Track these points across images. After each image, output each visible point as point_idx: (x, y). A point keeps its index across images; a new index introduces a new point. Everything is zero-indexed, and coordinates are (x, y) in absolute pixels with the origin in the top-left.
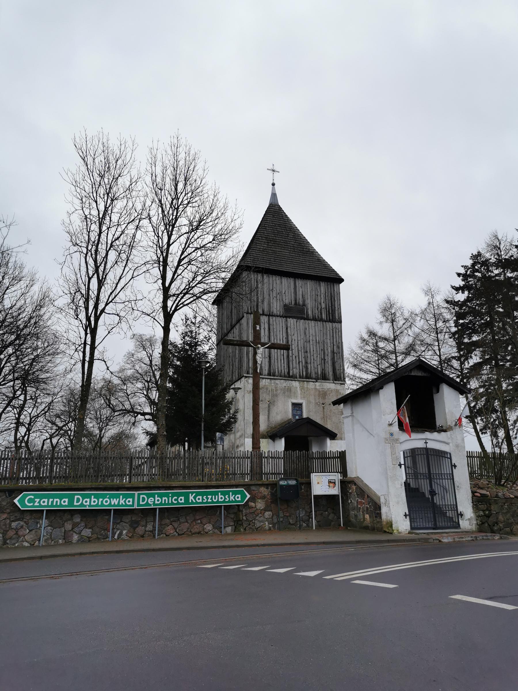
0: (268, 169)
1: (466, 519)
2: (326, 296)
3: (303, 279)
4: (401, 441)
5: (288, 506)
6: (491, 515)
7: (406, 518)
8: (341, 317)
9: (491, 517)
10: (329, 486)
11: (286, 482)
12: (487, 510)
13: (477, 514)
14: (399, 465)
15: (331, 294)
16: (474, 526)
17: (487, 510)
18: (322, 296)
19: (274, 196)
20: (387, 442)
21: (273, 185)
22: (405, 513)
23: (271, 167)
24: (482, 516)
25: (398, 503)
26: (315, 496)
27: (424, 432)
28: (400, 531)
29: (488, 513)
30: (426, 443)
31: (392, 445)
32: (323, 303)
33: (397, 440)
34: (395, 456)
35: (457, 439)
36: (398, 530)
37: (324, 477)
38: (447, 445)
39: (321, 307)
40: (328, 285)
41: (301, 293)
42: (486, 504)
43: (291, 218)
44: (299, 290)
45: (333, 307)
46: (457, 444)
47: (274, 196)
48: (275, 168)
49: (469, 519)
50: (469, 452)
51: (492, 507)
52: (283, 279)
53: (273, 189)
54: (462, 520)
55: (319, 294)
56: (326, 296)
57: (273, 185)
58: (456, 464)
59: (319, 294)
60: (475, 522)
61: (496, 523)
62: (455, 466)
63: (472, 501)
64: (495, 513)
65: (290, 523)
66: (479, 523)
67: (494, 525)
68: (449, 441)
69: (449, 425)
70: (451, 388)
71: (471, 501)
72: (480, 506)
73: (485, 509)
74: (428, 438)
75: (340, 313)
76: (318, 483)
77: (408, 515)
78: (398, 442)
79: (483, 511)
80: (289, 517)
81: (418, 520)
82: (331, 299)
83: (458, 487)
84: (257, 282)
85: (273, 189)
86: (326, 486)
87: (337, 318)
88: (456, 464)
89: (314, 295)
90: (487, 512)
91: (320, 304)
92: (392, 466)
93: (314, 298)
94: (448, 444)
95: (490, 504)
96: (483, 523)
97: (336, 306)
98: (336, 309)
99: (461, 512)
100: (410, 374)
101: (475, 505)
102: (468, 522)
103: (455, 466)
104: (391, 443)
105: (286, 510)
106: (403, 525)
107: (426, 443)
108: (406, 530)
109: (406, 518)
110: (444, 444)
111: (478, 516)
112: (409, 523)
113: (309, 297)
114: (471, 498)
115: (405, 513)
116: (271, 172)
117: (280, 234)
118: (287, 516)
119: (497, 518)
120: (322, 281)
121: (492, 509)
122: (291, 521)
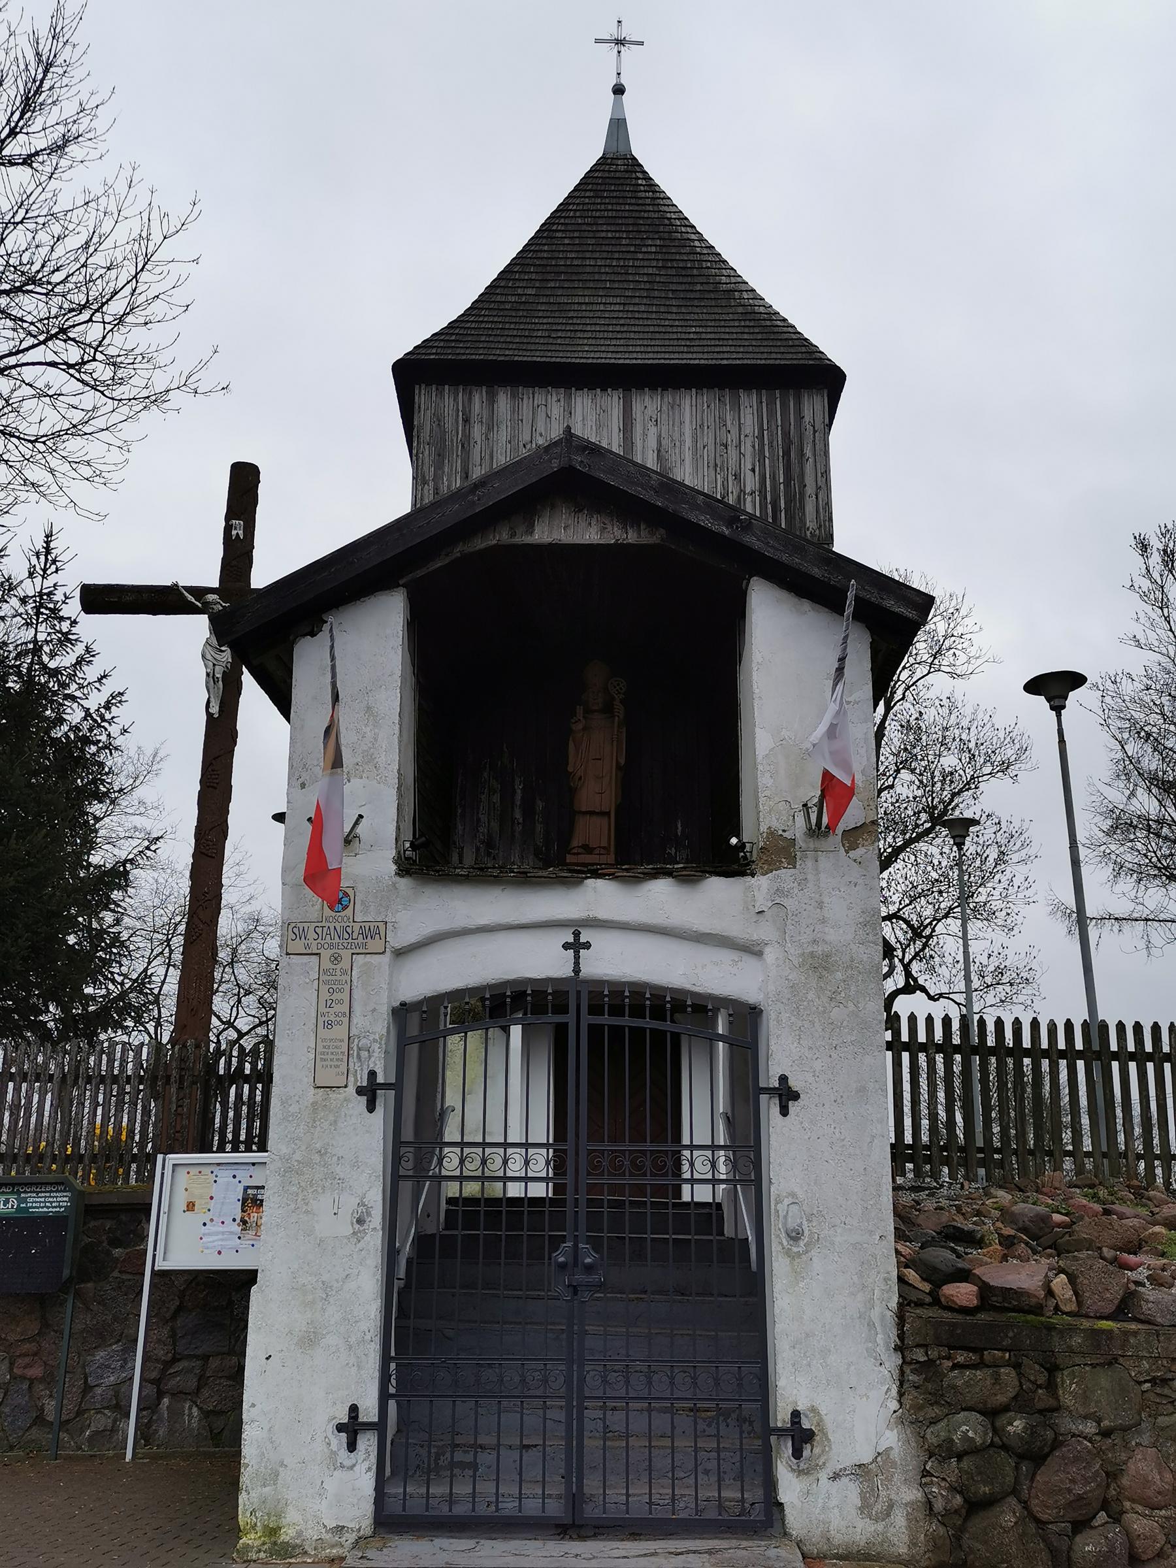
0: (597, 41)
1: (833, 1466)
2: (762, 445)
3: (665, 389)
4: (398, 940)
5: (45, 1325)
6: (1056, 1444)
7: (352, 1446)
8: (831, 520)
9: (1053, 1461)
10: (244, 1222)
11: (13, 1201)
12: (1020, 1403)
13: (934, 1435)
14: (360, 1091)
15: (786, 435)
16: (899, 1519)
17: (1020, 1403)
18: (747, 448)
19: (618, 126)
20: (298, 946)
21: (619, 90)
22: (354, 1409)
23: (611, 31)
24: (970, 1450)
25: (309, 1340)
26: (161, 1276)
27: (579, 882)
28: (287, 1535)
29: (1031, 1429)
30: (576, 946)
31: (325, 964)
32: (749, 474)
33: (370, 932)
34: (340, 1032)
35: (823, 921)
36: (273, 1532)
37: (224, 1176)
38: (749, 962)
39: (742, 491)
40: (771, 403)
41: (652, 443)
42: (1017, 1366)
43: (657, 181)
44: (645, 435)
45: (796, 484)
46: (819, 949)
47: (618, 126)
48: (626, 33)
49: (861, 1471)
50: (1138, 1027)
51: (1069, 1389)
52: (579, 400)
53: (618, 106)
54: (800, 1473)
55: (732, 438)
56: (762, 445)
57: (619, 90)
58: (794, 1083)
59: (732, 438)
60: (911, 1494)
61: (1105, 1505)
62: (786, 1095)
63: (901, 1337)
64: (1090, 1428)
65: (40, 1420)
66: (939, 1505)
67: (1080, 1525)
68: (763, 932)
69: (772, 833)
70: (806, 605)
71: (886, 1335)
72: (958, 1379)
73: (1002, 1399)
74: (602, 914)
75: (828, 505)
76: (191, 1207)
77: (368, 1426)
78: (375, 945)
79: (992, 1414)
80: (39, 1387)
81: (509, 1458)
82: (787, 453)
83: (795, 1236)
84: (466, 421)
85: (618, 106)
86: (228, 1221)
87: (811, 524)
88: (791, 1083)
89: (711, 447)
90: (1018, 1425)
91: (737, 477)
92: (311, 1095)
93: (707, 454)
94: (753, 950)
95: (1053, 1369)
96: (975, 1506)
97: (809, 480)
98: (810, 490)
99: (796, 1414)
100: (518, 540)
101: (928, 1367)
102: (850, 1492)
103: (786, 1095)
104: (326, 954)
105: (32, 1347)
106: (321, 1493)
107: (576, 946)
108: (340, 1529)
109: (352, 1446)
110: (726, 956)
111: (941, 1452)
112: (365, 1482)
113: (688, 456)
114: (890, 1318)
115: (354, 1409)
116: (610, 51)
117: (604, 248)
118: (32, 1381)
119: (1113, 1475)
120: (748, 387)
121: (1067, 1400)
122: (50, 1406)
